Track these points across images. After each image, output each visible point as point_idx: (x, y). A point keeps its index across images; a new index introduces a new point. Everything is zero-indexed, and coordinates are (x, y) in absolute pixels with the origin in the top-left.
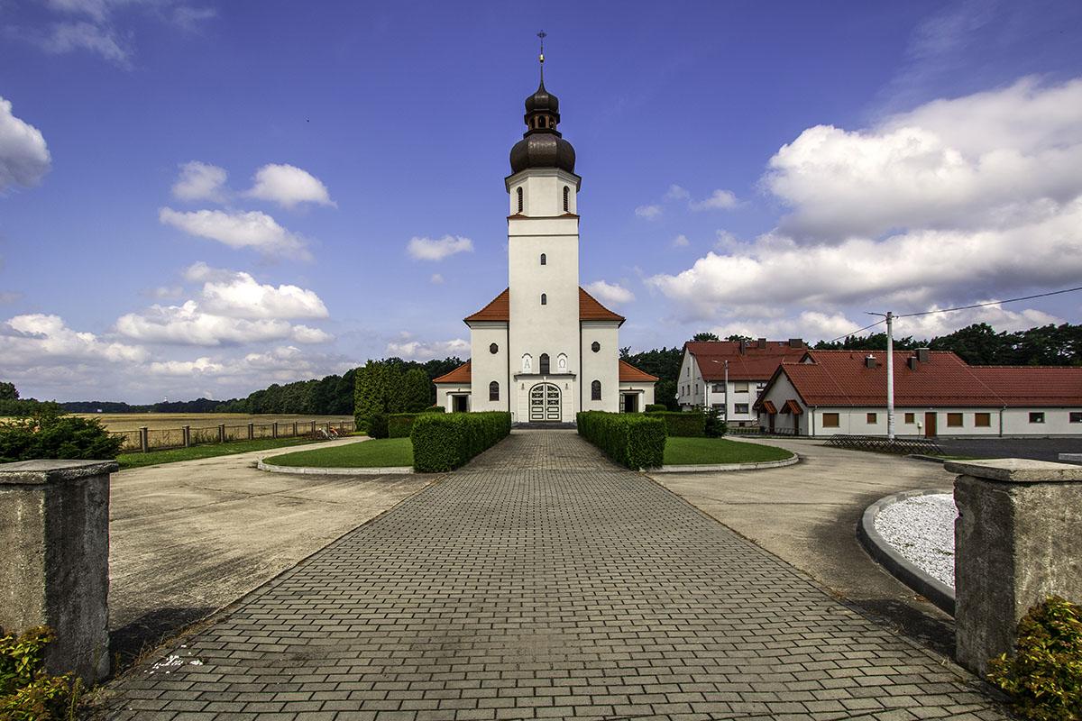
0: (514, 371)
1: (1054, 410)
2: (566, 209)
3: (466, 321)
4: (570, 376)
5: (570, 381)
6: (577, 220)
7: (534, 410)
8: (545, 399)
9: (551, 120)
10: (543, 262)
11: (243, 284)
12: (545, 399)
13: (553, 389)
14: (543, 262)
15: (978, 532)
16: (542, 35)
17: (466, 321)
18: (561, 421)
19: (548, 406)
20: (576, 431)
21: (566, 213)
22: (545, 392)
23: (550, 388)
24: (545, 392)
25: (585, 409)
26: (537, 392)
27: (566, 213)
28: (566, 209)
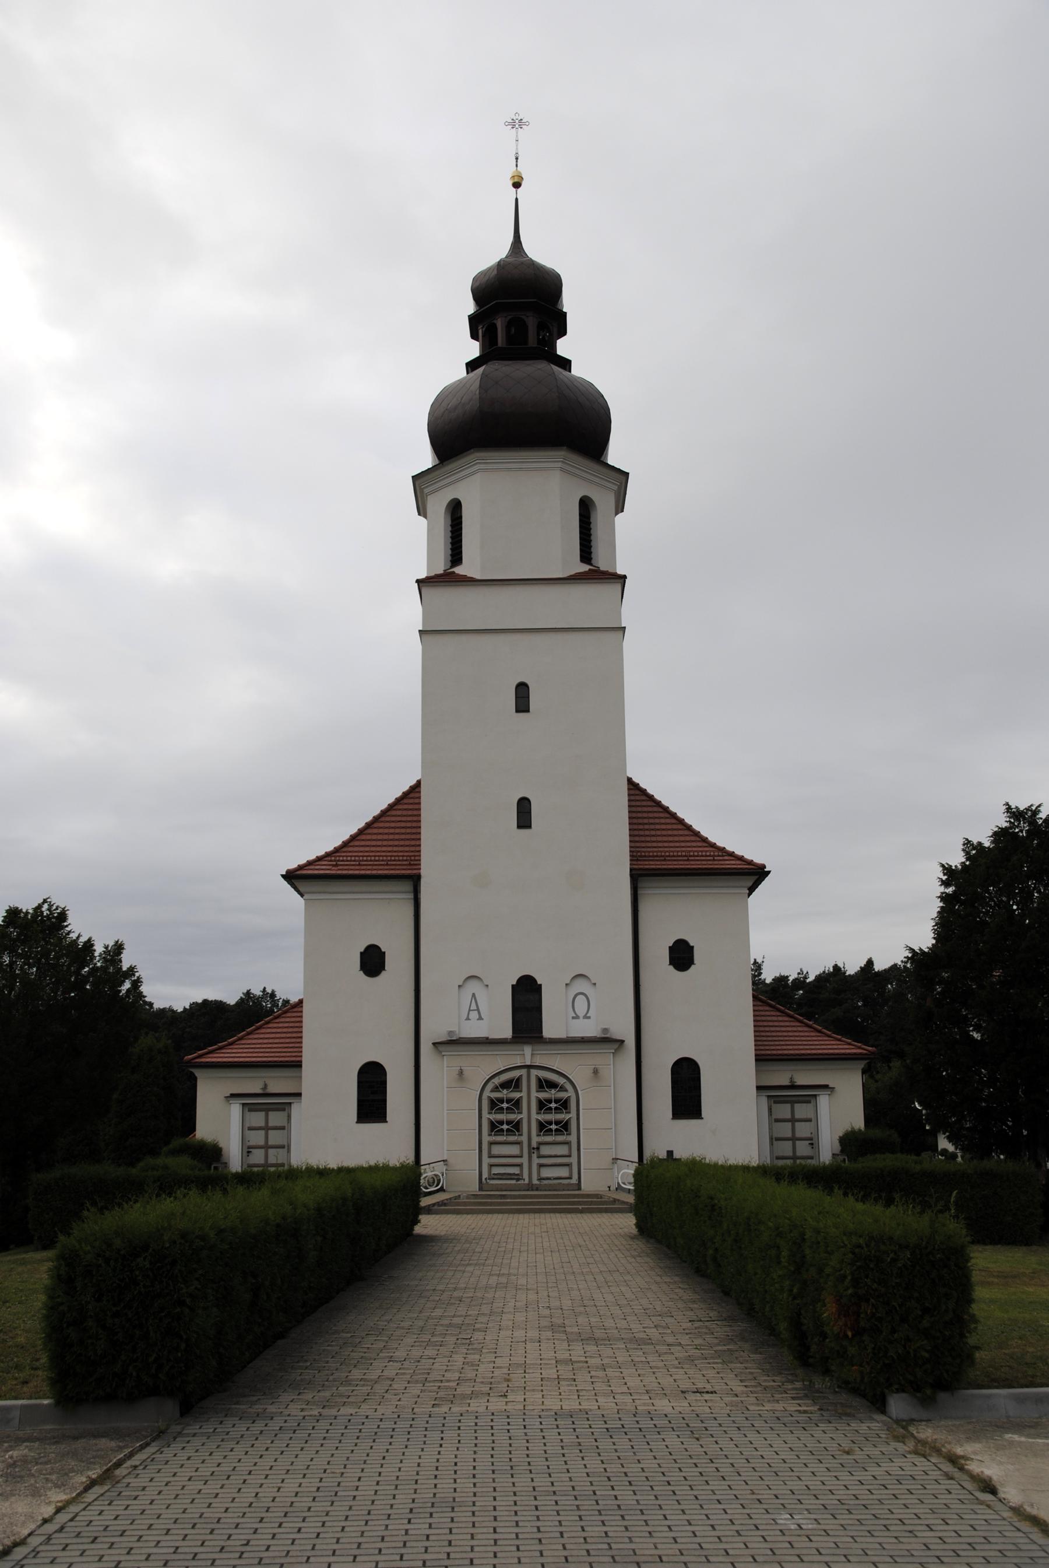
0: (433, 1029)
1: (210, 1070)
2: (586, 554)
3: (292, 877)
4: (607, 1041)
5: (603, 1058)
6: (619, 587)
7: (497, 1150)
8: (530, 1116)
9: (541, 327)
10: (522, 692)
11: (71, 919)
12: (530, 1116)
13: (552, 1085)
14: (522, 692)
15: (785, 1169)
16: (517, 124)
17: (292, 877)
18: (578, 1186)
19: (535, 1140)
20: (628, 1222)
21: (585, 568)
22: (530, 1095)
23: (544, 1084)
24: (530, 1095)
25: (657, 1148)
26: (504, 1094)
27: (585, 568)
28: (586, 554)
